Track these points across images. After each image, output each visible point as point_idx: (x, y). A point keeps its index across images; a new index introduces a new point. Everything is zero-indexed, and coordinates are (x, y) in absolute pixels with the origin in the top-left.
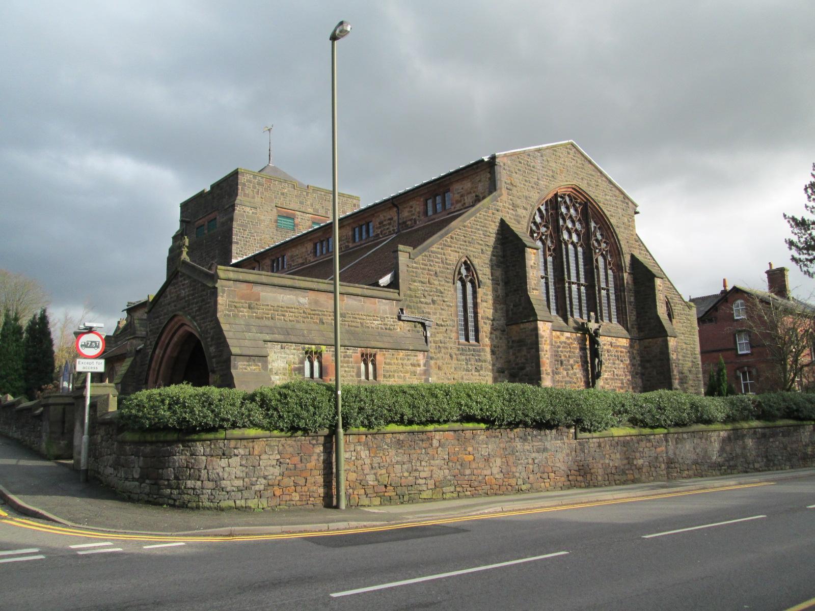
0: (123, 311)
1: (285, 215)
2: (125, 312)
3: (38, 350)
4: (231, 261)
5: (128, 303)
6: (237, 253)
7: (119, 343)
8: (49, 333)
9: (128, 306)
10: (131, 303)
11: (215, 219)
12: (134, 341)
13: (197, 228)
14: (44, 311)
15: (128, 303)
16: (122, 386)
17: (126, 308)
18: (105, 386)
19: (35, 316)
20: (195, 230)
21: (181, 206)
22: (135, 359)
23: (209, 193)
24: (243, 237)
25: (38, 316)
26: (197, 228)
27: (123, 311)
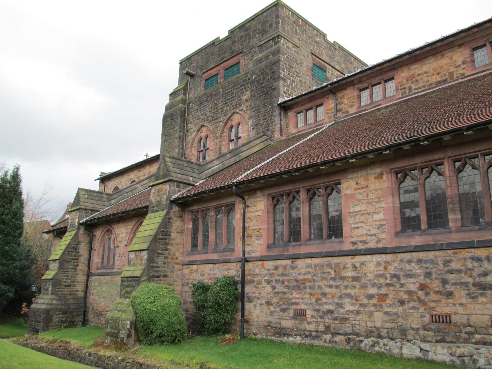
0: (96, 180)
1: (318, 65)
2: (99, 181)
3: (7, 211)
4: (278, 100)
5: (102, 173)
6: (284, 92)
7: (113, 202)
8: (21, 194)
9: (100, 176)
10: (104, 173)
11: (239, 63)
12: (167, 187)
13: (206, 80)
14: (18, 169)
15: (102, 173)
16: (148, 254)
17: (99, 177)
18: (332, 242)
19: (6, 173)
20: (203, 82)
21: (181, 63)
22: (168, 214)
23: (226, 39)
24: (289, 74)
25: (10, 174)
26: (206, 80)
27: (96, 180)
